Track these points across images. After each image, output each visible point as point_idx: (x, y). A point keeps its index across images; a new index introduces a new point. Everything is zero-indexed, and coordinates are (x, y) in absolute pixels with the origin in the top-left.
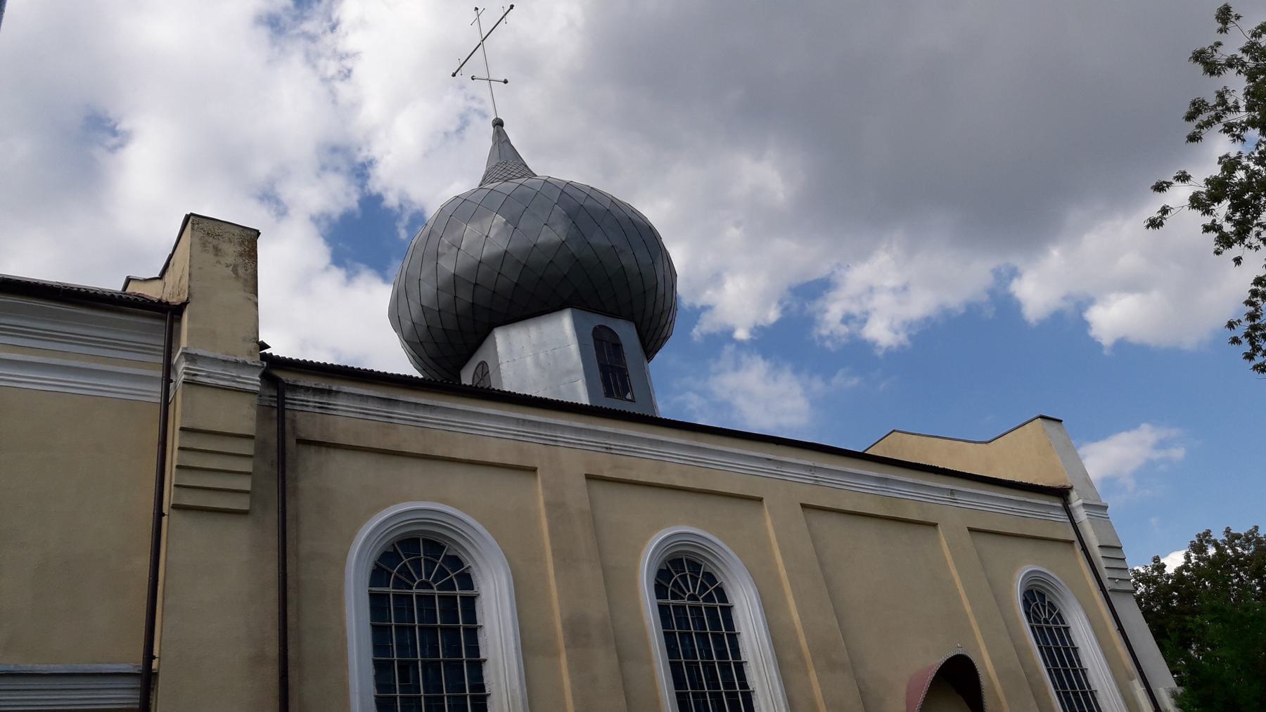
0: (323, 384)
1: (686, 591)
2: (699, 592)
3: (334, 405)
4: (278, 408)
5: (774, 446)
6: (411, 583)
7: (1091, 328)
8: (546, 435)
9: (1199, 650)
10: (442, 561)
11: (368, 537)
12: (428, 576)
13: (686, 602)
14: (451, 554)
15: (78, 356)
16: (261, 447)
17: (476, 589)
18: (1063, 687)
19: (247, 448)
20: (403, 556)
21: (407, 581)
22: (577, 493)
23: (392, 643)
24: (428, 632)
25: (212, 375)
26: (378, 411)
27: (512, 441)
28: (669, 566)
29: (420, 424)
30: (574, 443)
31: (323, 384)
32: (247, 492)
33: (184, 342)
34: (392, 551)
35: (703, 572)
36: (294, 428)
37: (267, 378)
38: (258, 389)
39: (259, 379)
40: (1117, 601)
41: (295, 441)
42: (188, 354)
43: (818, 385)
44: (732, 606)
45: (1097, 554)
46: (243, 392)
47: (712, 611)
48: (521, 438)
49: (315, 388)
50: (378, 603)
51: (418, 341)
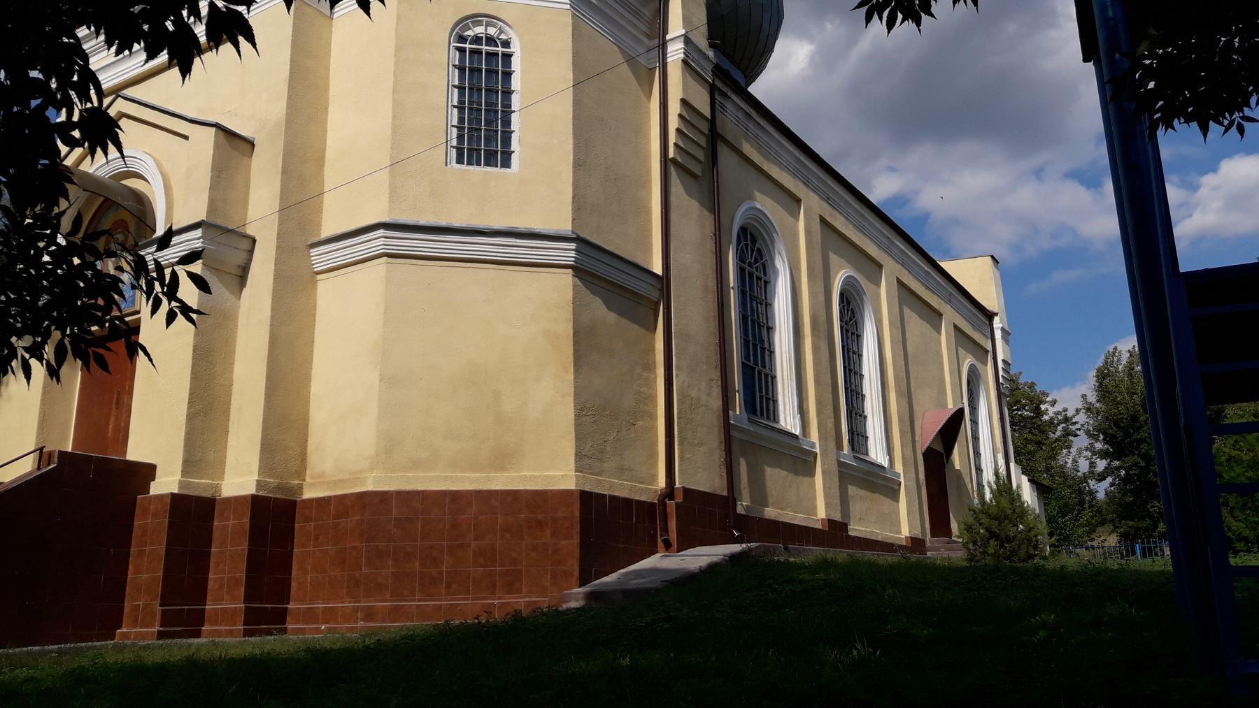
45: (1000, 365)
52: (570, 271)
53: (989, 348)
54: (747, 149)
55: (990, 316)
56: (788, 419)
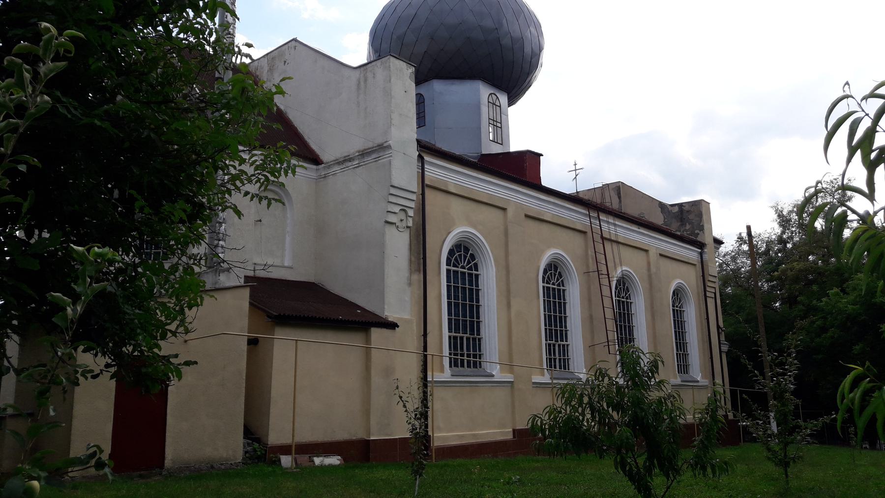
1: (463, 263)
9: (145, 257)
40: (708, 299)
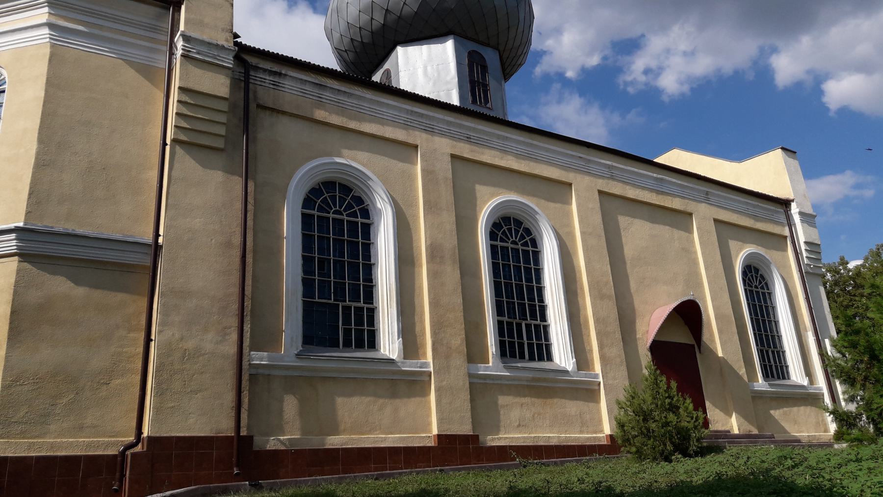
0: (276, 68)
2: (519, 239)
3: (283, 84)
4: (245, 81)
5: (585, 148)
6: (329, 210)
7: (824, 96)
8: (426, 124)
10: (350, 199)
11: (303, 175)
12: (341, 207)
13: (510, 246)
14: (356, 195)
15: (110, 29)
16: (233, 107)
17: (371, 219)
18: (759, 330)
19: (224, 106)
20: (325, 192)
21: (328, 209)
22: (445, 167)
23: (315, 245)
24: (339, 243)
25: (201, 52)
26: (312, 92)
27: (402, 125)
28: (501, 221)
29: (340, 105)
30: (445, 132)
31: (276, 68)
32: (222, 136)
33: (182, 27)
34: (318, 188)
35: (523, 228)
36: (256, 97)
37: (237, 58)
38: (231, 66)
39: (232, 59)
41: (256, 106)
42: (185, 35)
43: (616, 118)
44: (540, 251)
46: (221, 67)
47: (526, 253)
48: (409, 124)
49: (271, 71)
50: (307, 220)
51: (344, 50)
52: (16, 258)
53: (787, 232)
54: (320, 114)
55: (785, 204)
56: (797, 375)
